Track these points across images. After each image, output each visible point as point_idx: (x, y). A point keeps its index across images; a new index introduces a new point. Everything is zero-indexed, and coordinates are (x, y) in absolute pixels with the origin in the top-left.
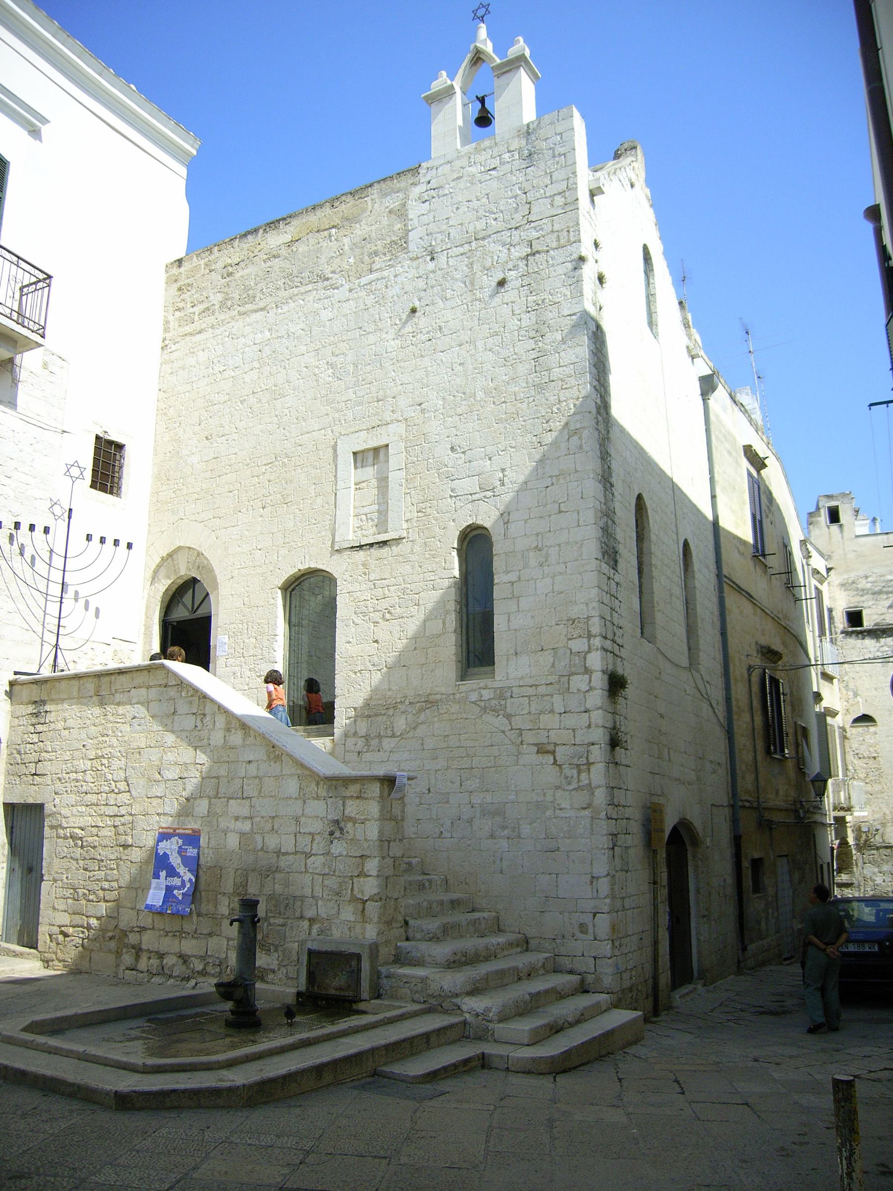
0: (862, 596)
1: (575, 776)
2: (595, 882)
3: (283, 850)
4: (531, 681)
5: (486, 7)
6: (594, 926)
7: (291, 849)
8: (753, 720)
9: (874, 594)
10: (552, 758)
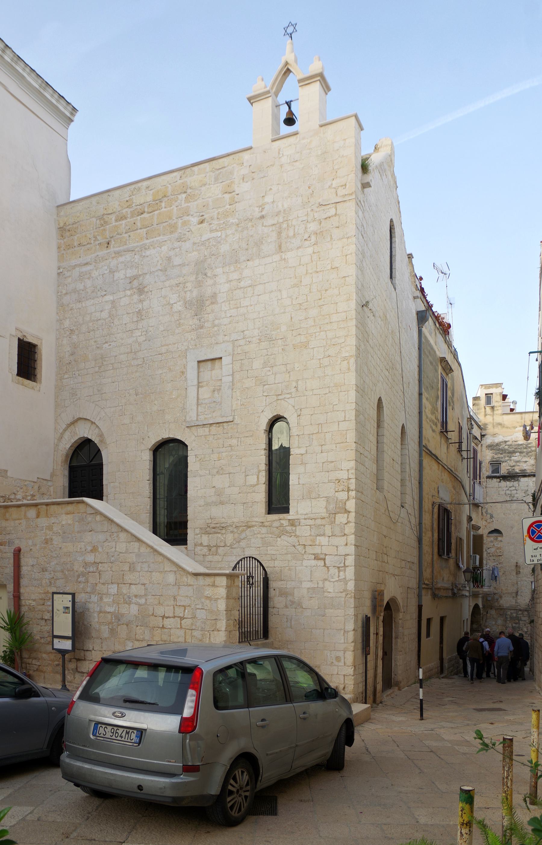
0: (501, 454)
1: (337, 574)
2: (346, 635)
3: (166, 615)
4: (312, 516)
5: (294, 26)
6: (344, 658)
7: (171, 615)
8: (433, 536)
9: (509, 453)
10: (323, 562)
